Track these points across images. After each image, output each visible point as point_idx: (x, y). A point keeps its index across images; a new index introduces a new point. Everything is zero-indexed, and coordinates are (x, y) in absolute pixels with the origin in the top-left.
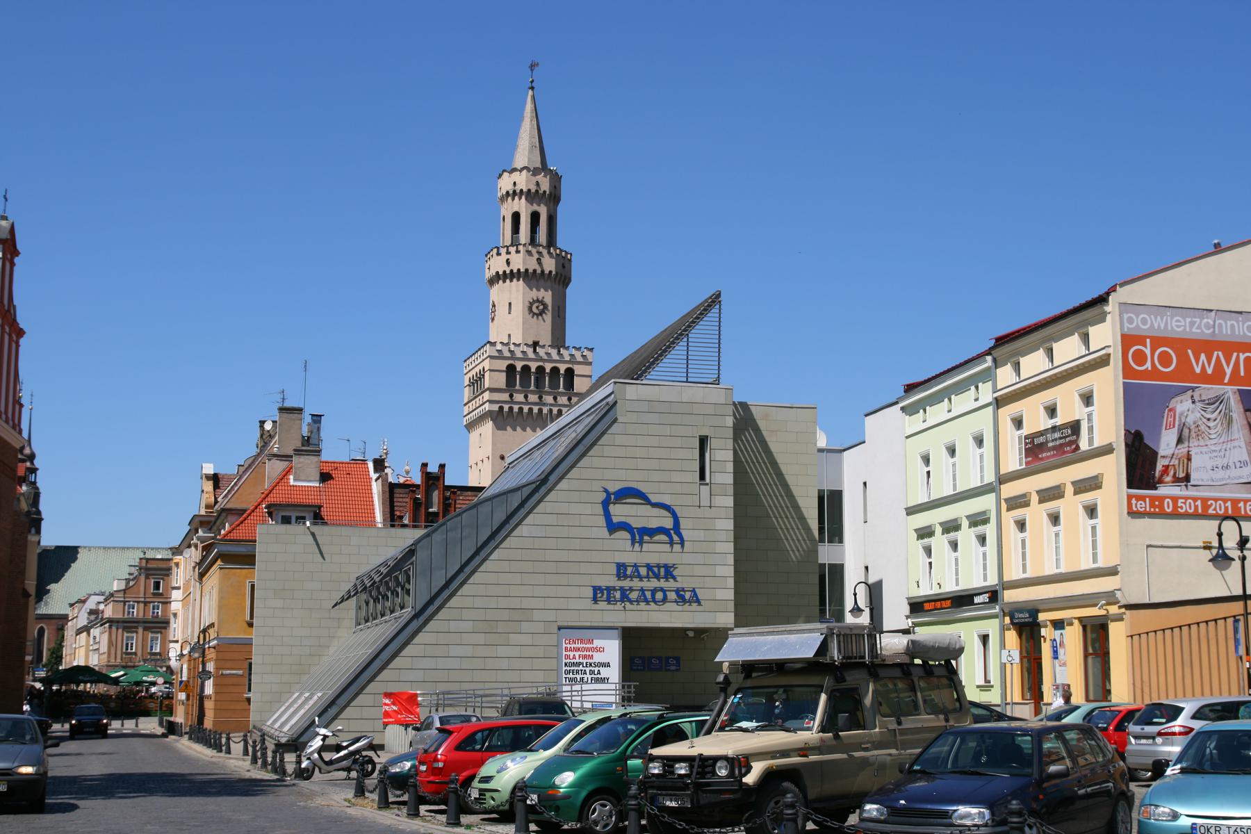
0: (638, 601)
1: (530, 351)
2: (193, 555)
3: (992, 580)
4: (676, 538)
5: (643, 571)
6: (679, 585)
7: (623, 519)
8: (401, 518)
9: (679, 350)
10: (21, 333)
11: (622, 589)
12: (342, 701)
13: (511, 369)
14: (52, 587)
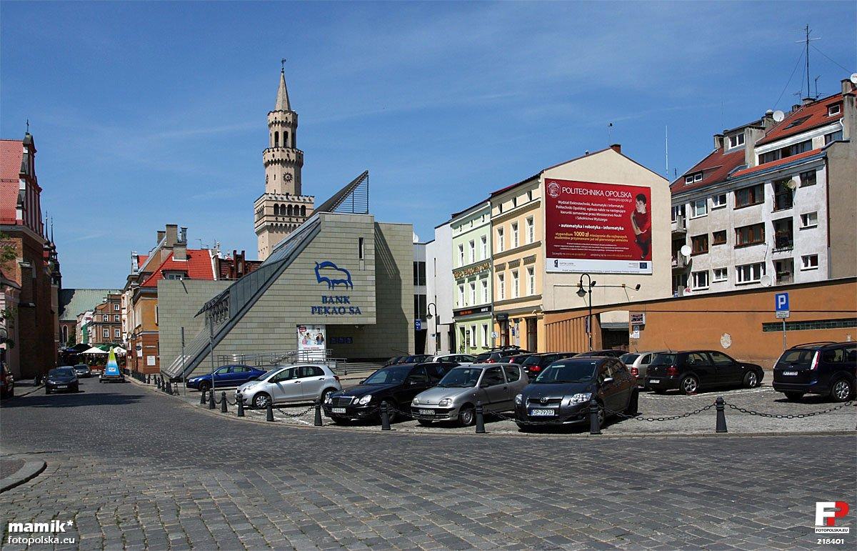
0: (332, 313)
1: (285, 197)
2: (129, 294)
3: (489, 301)
4: (349, 284)
5: (334, 299)
6: (350, 305)
7: (323, 276)
8: (225, 276)
9: (349, 199)
10: (40, 190)
11: (325, 307)
12: (199, 359)
13: (276, 206)
14: (65, 307)
